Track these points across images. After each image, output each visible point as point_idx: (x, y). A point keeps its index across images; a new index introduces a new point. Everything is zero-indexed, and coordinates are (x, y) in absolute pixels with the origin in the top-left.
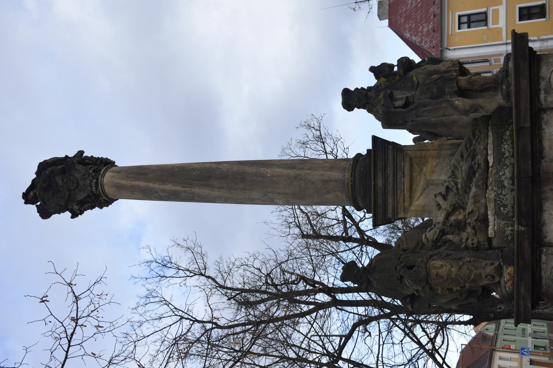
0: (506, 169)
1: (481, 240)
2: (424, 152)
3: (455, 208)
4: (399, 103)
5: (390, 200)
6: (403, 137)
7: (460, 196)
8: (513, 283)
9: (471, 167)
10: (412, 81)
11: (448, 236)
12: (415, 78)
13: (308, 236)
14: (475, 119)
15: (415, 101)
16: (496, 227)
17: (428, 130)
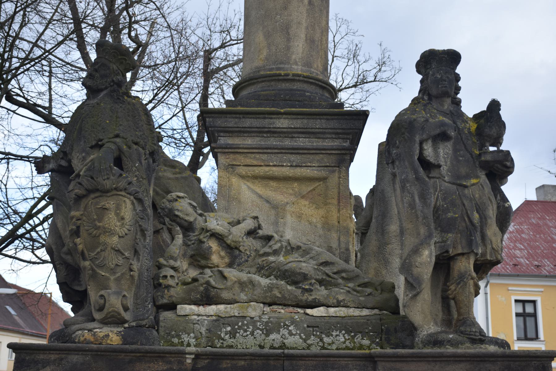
0: (301, 338)
1: (172, 292)
2: (335, 202)
3: (232, 250)
4: (429, 151)
5: (249, 141)
6: (362, 176)
7: (254, 259)
8: (89, 342)
9: (305, 277)
10: (468, 177)
11: (181, 236)
12: (474, 181)
13: (208, 55)
14: (394, 287)
15: (432, 180)
16: (195, 317)
17: (374, 220)
